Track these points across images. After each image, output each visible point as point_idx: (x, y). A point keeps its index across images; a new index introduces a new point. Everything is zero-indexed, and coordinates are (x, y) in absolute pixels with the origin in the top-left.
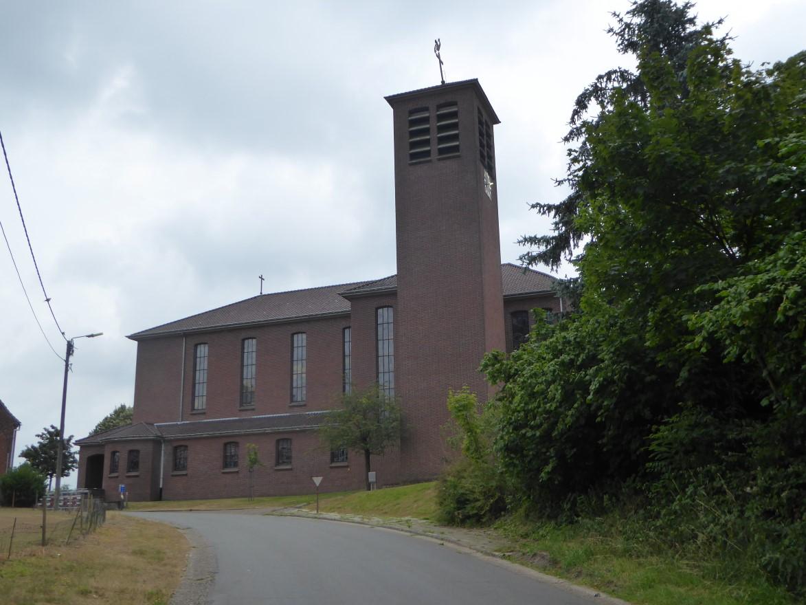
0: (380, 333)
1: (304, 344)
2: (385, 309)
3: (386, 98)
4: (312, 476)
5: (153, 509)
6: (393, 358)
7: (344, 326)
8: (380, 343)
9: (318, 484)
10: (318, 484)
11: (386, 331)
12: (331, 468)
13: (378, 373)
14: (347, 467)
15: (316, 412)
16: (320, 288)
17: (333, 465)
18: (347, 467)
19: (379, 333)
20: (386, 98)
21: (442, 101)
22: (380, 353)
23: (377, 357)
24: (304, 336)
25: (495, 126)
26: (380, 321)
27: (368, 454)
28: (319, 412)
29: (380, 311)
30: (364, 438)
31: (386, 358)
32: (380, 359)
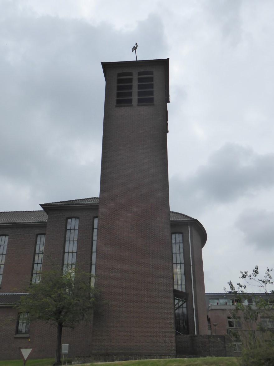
0: (68, 236)
1: (6, 243)
2: (73, 220)
3: (102, 63)
4: (20, 348)
5: (209, 295)
6: (75, 254)
7: (38, 233)
8: (67, 243)
9: (26, 357)
10: (26, 357)
11: (72, 235)
12: (15, 338)
13: (63, 265)
14: (29, 338)
15: (8, 294)
16: (20, 212)
17: (18, 336)
18: (29, 338)
19: (67, 236)
20: (102, 63)
21: (142, 70)
22: (66, 250)
23: (64, 253)
24: (7, 238)
25: (168, 103)
26: (68, 227)
27: (60, 326)
28: (10, 294)
29: (69, 220)
30: (59, 312)
31: (70, 255)
32: (66, 255)
